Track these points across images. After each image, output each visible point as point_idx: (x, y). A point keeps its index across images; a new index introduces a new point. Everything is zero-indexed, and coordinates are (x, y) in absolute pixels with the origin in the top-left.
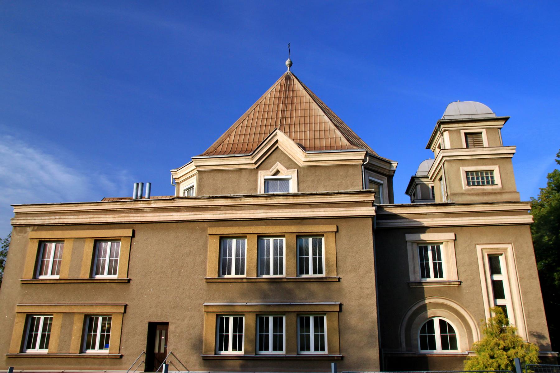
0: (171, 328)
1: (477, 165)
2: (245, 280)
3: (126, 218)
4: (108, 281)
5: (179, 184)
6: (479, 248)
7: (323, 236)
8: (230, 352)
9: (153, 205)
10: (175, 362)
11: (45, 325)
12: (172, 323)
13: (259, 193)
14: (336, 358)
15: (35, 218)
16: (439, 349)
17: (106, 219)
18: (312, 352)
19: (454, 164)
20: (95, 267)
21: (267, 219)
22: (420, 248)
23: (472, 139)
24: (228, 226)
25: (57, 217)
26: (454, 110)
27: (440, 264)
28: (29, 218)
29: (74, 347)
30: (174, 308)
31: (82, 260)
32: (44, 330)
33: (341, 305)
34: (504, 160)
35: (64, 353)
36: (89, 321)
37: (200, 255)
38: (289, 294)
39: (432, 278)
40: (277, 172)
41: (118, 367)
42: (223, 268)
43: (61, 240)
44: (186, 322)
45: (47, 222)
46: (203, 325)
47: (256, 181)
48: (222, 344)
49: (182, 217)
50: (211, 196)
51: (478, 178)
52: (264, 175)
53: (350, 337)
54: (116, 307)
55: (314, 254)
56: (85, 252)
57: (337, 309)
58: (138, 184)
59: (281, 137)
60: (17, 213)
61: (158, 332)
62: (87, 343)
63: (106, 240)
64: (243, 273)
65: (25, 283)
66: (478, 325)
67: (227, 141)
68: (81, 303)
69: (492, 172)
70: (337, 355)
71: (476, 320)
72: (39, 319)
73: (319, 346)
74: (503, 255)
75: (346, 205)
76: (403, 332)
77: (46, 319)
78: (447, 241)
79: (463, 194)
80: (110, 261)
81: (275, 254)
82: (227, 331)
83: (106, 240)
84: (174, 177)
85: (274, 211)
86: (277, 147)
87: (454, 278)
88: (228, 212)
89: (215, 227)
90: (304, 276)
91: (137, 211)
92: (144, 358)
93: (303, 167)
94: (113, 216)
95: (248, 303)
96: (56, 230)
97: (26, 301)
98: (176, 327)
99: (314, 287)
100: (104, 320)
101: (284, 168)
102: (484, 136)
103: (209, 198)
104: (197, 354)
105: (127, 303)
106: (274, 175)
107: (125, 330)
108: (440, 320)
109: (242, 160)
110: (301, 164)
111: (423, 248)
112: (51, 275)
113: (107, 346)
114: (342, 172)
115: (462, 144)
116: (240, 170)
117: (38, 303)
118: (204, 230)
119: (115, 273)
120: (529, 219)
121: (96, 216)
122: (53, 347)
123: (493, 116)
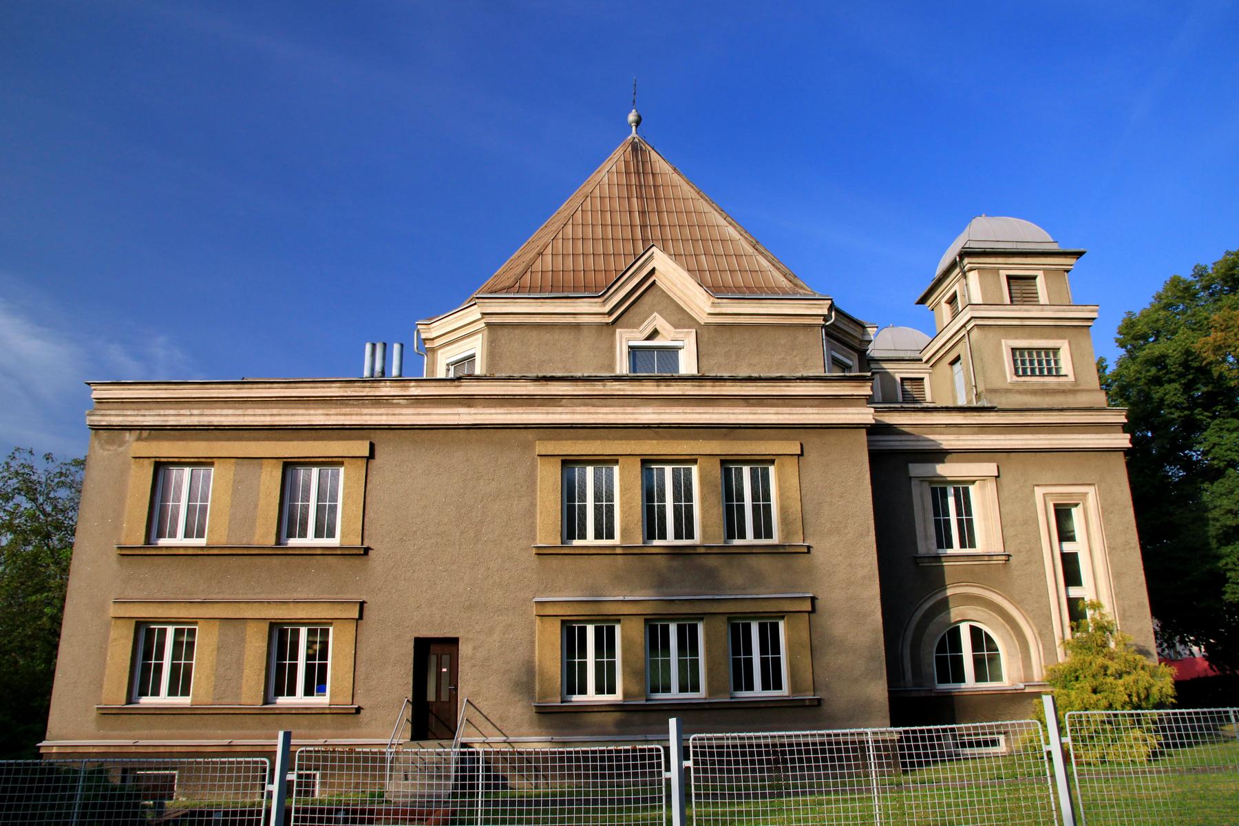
0: (464, 649)
1: (1031, 337)
2: (619, 551)
3: (354, 417)
4: (319, 552)
5: (433, 350)
6: (1039, 492)
7: (772, 462)
8: (591, 696)
9: (414, 390)
10: (478, 719)
11: (177, 645)
12: (467, 639)
13: (618, 372)
14: (807, 703)
15: (143, 412)
16: (970, 682)
17: (308, 418)
18: (758, 692)
19: (991, 334)
20: (289, 522)
21: (659, 426)
22: (934, 491)
23: (1020, 286)
24: (578, 439)
25: (195, 412)
26: (984, 230)
27: (970, 522)
28: (129, 412)
29: (251, 689)
30: (470, 607)
31: (256, 506)
32: (176, 656)
33: (813, 599)
34: (1077, 330)
35: (228, 702)
36: (281, 638)
37: (520, 497)
38: (710, 576)
39: (956, 549)
40: (654, 334)
41: (351, 731)
42: (572, 525)
43: (206, 462)
44: (496, 636)
45: (172, 421)
46: (533, 642)
47: (612, 348)
48: (573, 682)
49: (479, 417)
50: (540, 375)
51: (1031, 362)
52: (626, 338)
53: (834, 660)
54: (340, 607)
55: (755, 497)
56: (262, 487)
57: (807, 606)
58: (374, 346)
59: (661, 261)
60: (100, 401)
61: (433, 659)
62: (281, 682)
63: (309, 463)
64: (331, 534)
65: (127, 553)
66: (1040, 634)
67: (538, 266)
68: (262, 597)
69: (1056, 350)
70: (809, 696)
71: (1037, 626)
72: (163, 633)
73: (772, 678)
74: (1080, 506)
75: (816, 402)
76: (907, 652)
77: (178, 633)
78: (984, 478)
79: (1007, 391)
80: (190, 510)
81: (677, 498)
82: (583, 653)
83: (309, 463)
84: (423, 336)
85: (675, 410)
86: (654, 283)
87: (997, 548)
88: (579, 409)
89: (551, 439)
90: (737, 542)
91: (378, 401)
92: (408, 713)
93: (707, 325)
94: (325, 411)
95: (631, 596)
96: (192, 440)
97: (131, 594)
98: (474, 648)
99: (762, 563)
100: (311, 633)
101: (668, 326)
102: (1040, 282)
103: (538, 379)
104: (525, 703)
105: (364, 598)
106: (649, 338)
107: (362, 656)
108: (972, 628)
109: (583, 306)
110: (703, 319)
111: (938, 490)
112: (185, 537)
113: (322, 690)
114: (783, 339)
115: (1002, 298)
116: (577, 326)
117: (159, 596)
118: (528, 446)
119: (200, 535)
120: (1124, 441)
121: (285, 411)
122: (201, 691)
123: (1055, 247)
